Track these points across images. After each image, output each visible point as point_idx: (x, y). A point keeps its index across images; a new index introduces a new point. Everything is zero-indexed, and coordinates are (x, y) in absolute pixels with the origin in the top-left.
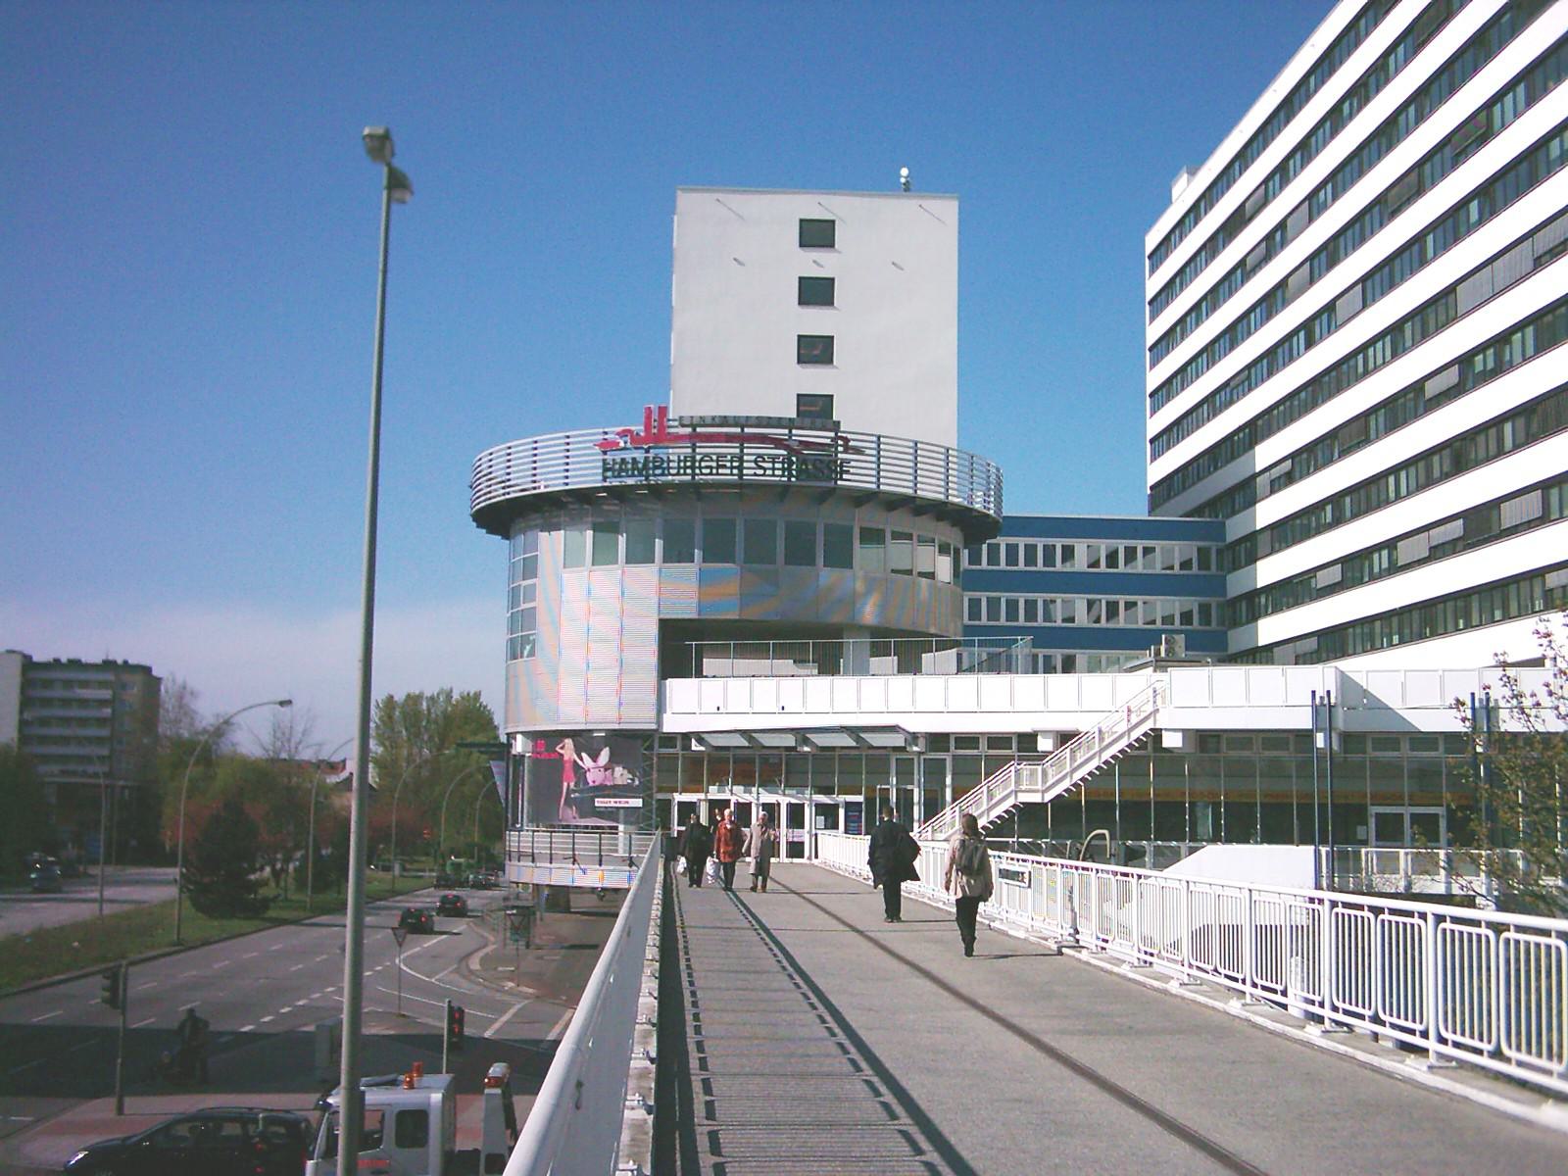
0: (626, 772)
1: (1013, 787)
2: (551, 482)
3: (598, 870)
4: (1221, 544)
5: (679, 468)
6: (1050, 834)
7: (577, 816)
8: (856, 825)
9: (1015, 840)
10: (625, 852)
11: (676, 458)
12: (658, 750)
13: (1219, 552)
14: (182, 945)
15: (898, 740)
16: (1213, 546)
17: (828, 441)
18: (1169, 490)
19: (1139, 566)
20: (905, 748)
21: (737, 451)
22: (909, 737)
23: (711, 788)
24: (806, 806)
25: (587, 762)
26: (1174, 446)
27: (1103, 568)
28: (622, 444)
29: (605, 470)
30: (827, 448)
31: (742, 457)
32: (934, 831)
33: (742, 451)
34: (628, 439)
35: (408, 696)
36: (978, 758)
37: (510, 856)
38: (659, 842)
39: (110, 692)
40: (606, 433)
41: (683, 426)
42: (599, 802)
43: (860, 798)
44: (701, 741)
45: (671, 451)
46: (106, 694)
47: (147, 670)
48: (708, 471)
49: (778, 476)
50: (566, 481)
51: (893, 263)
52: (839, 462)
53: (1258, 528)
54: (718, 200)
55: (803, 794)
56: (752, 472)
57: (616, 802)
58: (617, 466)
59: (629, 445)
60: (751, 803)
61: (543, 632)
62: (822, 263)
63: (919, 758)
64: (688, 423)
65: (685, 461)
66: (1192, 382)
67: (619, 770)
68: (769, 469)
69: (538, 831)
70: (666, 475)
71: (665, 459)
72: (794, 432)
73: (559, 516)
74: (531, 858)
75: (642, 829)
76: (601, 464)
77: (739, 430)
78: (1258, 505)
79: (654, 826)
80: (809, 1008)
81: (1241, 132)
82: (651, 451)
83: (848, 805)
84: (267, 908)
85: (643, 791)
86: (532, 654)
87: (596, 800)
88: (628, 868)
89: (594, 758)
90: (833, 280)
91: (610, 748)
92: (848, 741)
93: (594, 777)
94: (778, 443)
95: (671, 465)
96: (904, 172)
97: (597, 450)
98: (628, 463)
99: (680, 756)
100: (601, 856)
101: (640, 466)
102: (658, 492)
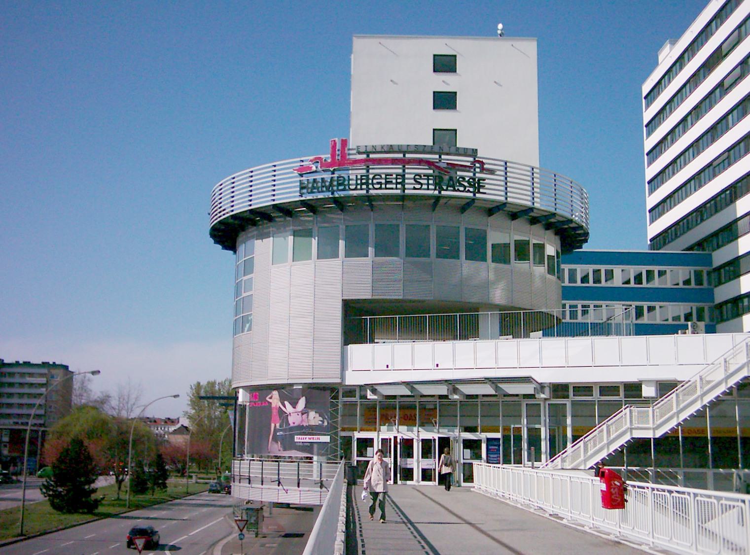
0: (317, 415)
1: (628, 425)
2: (262, 201)
3: (295, 490)
4: (709, 269)
5: (357, 184)
6: (653, 464)
7: (281, 449)
8: (495, 456)
9: (625, 468)
10: (317, 477)
11: (354, 177)
12: (342, 399)
13: (709, 273)
14: (25, 536)
15: (528, 389)
16: (705, 270)
17: (469, 164)
18: (665, 240)
19: (656, 283)
20: (534, 395)
21: (400, 171)
22: (538, 387)
23: (382, 427)
24: (414, 440)
25: (289, 408)
26: (667, 211)
27: (632, 284)
28: (314, 168)
29: (302, 188)
30: (468, 169)
31: (404, 175)
32: (563, 461)
33: (404, 171)
34: (319, 165)
35: (209, 383)
36: (592, 403)
37: (234, 479)
38: (343, 469)
39: (45, 379)
40: (302, 161)
41: (359, 153)
42: (298, 439)
43: (498, 435)
44: (374, 391)
45: (350, 172)
46: (43, 380)
47: (66, 367)
48: (379, 186)
49: (432, 189)
50: (273, 198)
51: (495, 82)
52: (477, 179)
53: (740, 254)
54: (380, 43)
55: (453, 432)
56: (412, 186)
57: (310, 439)
58: (310, 185)
59: (319, 169)
60: (412, 440)
61: (256, 314)
62: (448, 82)
63: (545, 403)
64: (364, 150)
65: (361, 179)
66: (681, 168)
67: (312, 414)
68: (425, 184)
69: (254, 460)
70: (347, 190)
71: (347, 178)
72: (443, 157)
73: (269, 227)
74: (248, 480)
75: (330, 459)
76: (298, 184)
77: (401, 156)
78: (740, 240)
79: (339, 457)
80: (413, 538)
81: (652, 80)
82: (336, 172)
83: (488, 440)
84: (97, 507)
85: (331, 429)
86: (250, 329)
87: (296, 437)
88: (319, 489)
89: (294, 405)
90: (456, 93)
91: (306, 398)
92: (489, 390)
93: (294, 419)
94: (429, 163)
95: (351, 182)
96: (500, 26)
97: (296, 174)
98: (319, 182)
99: (359, 403)
100: (299, 480)
101: (327, 184)
102: (340, 204)
